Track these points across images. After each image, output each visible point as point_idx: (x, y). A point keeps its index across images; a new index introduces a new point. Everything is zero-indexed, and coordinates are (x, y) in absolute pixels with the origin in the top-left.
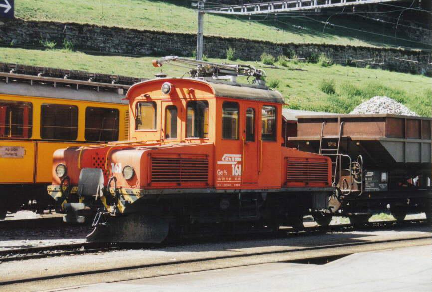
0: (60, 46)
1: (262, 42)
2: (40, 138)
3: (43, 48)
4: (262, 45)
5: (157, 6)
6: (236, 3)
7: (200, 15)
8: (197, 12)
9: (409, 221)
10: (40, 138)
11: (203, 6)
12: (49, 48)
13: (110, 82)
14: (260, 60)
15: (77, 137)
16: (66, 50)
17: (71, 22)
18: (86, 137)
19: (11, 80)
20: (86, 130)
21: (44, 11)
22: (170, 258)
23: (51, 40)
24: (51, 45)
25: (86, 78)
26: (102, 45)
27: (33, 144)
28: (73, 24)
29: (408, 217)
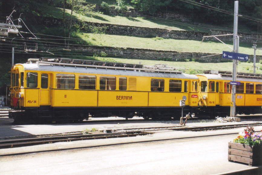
0: (191, 60)
1: (259, 56)
2: (99, 89)
3: (185, 61)
4: (259, 57)
5: (220, 45)
6: (182, 32)
7: (255, 50)
8: (254, 49)
9: (84, 121)
10: (99, 89)
11: (256, 47)
12: (187, 61)
13: (259, 76)
14: (259, 62)
15: (126, 89)
16: (193, 62)
17: (194, 52)
18: (120, 89)
19: (249, 77)
20: (170, 88)
21: (185, 49)
22: (59, 146)
23: (188, 59)
24: (188, 60)
25: (254, 75)
26: (204, 59)
27: (96, 92)
28: (195, 53)
29: (129, 119)
